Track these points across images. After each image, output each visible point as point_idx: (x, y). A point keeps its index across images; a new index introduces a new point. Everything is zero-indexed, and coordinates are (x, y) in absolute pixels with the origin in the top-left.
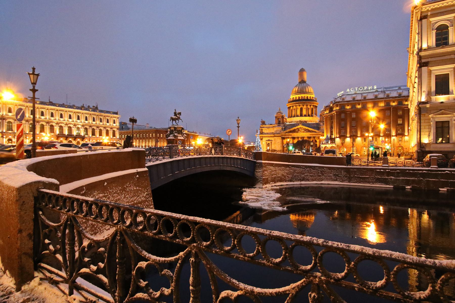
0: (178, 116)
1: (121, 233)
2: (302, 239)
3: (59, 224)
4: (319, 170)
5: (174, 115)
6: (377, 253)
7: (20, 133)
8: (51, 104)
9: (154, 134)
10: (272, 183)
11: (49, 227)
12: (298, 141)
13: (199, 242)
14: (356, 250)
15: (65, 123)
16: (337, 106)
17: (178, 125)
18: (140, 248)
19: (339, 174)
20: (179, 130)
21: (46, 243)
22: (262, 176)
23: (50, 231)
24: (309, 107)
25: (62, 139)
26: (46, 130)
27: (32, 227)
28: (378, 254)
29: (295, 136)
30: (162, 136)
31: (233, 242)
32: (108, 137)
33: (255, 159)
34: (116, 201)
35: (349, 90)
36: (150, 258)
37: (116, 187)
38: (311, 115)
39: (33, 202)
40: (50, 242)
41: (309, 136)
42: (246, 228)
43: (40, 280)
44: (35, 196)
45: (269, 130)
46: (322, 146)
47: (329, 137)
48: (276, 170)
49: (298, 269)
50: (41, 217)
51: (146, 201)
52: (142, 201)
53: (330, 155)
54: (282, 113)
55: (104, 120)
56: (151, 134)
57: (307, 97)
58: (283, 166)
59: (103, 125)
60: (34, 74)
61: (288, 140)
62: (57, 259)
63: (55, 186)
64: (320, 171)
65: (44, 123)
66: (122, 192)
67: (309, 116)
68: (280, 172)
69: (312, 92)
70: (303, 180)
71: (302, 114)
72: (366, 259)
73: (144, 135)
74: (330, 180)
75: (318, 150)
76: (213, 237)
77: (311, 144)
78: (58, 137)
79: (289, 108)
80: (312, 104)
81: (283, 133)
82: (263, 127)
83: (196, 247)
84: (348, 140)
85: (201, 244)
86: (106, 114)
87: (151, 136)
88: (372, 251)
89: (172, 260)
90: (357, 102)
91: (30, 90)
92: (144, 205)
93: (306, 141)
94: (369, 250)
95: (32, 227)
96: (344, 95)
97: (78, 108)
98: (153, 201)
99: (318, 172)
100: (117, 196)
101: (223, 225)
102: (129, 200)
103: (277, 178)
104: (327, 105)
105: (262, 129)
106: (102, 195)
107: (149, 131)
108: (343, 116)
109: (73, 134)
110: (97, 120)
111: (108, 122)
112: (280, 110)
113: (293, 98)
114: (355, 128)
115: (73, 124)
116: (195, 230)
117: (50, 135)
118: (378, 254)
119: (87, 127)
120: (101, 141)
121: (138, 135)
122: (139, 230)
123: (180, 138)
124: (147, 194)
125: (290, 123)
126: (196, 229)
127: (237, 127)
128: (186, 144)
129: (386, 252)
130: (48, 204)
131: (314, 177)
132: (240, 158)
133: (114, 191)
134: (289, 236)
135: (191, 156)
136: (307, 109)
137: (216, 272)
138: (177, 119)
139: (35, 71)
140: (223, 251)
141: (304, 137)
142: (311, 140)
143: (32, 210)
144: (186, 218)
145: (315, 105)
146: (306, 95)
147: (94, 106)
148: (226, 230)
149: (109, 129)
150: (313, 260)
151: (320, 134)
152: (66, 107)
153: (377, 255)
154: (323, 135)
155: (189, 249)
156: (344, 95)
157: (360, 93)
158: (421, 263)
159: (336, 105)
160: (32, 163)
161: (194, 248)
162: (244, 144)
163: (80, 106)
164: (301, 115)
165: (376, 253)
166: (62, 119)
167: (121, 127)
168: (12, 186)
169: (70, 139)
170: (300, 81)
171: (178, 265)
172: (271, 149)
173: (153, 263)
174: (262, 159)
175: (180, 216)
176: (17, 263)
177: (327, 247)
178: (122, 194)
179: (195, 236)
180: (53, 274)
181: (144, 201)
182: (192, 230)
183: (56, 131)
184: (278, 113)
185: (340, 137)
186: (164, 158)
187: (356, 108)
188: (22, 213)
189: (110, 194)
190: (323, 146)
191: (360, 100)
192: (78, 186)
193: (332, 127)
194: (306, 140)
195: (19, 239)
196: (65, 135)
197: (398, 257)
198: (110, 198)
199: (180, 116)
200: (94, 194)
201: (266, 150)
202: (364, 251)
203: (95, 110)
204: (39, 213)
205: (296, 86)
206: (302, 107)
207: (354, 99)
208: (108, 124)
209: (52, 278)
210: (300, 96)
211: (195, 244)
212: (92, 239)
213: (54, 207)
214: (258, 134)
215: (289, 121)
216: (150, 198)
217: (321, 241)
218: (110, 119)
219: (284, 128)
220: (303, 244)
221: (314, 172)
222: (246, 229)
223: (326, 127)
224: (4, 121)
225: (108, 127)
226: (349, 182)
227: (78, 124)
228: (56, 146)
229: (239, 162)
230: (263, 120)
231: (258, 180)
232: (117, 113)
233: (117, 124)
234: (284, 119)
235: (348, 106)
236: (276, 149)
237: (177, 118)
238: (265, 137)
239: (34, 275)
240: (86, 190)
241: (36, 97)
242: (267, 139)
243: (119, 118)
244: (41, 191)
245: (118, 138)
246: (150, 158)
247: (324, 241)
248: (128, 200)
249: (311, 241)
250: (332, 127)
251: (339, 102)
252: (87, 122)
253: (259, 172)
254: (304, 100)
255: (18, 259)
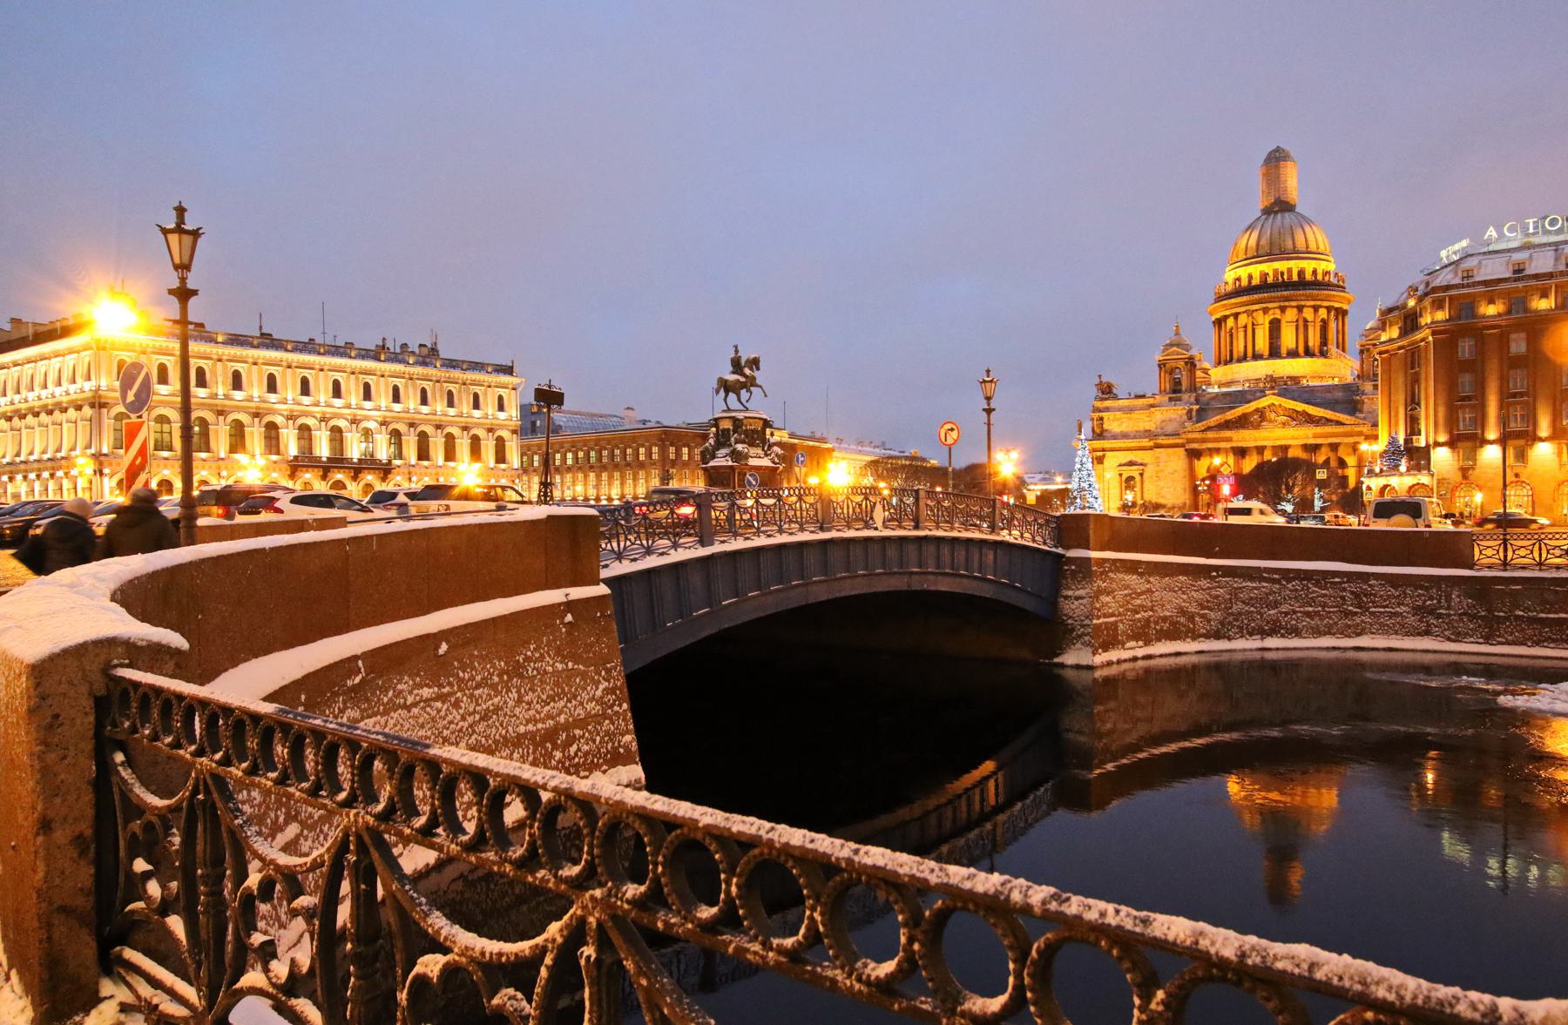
0: (747, 371)
1: (359, 837)
2: (967, 885)
3: (174, 800)
4: (1345, 590)
5: (731, 369)
6: (1254, 954)
7: (135, 458)
8: (268, 341)
9: (655, 449)
10: (1132, 644)
11: (145, 812)
12: (1260, 467)
13: (610, 884)
14: (1171, 938)
15: (318, 416)
16: (1438, 305)
17: (747, 409)
18: (423, 900)
19: (1441, 607)
20: (754, 431)
21: (136, 874)
22: (1090, 616)
23: (149, 827)
24: (1308, 314)
25: (308, 476)
26: (253, 445)
27: (89, 810)
28: (1258, 960)
29: (1244, 444)
30: (689, 454)
31: (723, 886)
32: (478, 466)
33: (1060, 542)
34: (486, 715)
35: (1494, 234)
36: (454, 942)
37: (483, 659)
38: (1317, 351)
39: (92, 718)
40: (150, 867)
41: (1312, 441)
42: (767, 833)
43: (121, 1011)
44: (98, 694)
45: (1129, 419)
46: (1367, 482)
47: (1402, 442)
48: (1149, 591)
49: (955, 1008)
50: (118, 772)
51: (605, 716)
52: (589, 715)
53: (1400, 523)
54: (1187, 348)
55: (460, 399)
56: (642, 450)
57: (1301, 273)
58: (1182, 574)
59: (429, 417)
60: (183, 230)
61: (1217, 460)
62: (169, 934)
63: (171, 658)
64: (1352, 593)
65: (244, 418)
66: (507, 682)
67: (1308, 353)
68: (1169, 598)
69: (1322, 248)
70: (1272, 632)
71: (1279, 347)
72: (1211, 979)
73: (617, 452)
74: (1396, 633)
75: (1352, 501)
76: (656, 864)
77: (1319, 477)
78: (295, 467)
79: (1219, 323)
80: (1326, 304)
81: (1194, 430)
82: (1107, 409)
83: (604, 904)
84: (1491, 454)
85: (618, 890)
86: (471, 376)
87: (642, 458)
88: (1237, 944)
89: (523, 951)
90: (1533, 283)
91: (171, 292)
92: (598, 734)
93: (1296, 464)
94: (1226, 939)
95: (90, 812)
96: (1472, 255)
97: (365, 354)
98: (634, 717)
99: (1343, 598)
100: (489, 695)
101: (690, 818)
102: (536, 711)
103: (1156, 623)
104: (1390, 303)
105: (1101, 419)
106: (431, 690)
107: (634, 439)
108: (1466, 348)
109: (349, 456)
110: (438, 398)
111: (476, 406)
112: (1177, 334)
113: (1239, 279)
114: (1527, 403)
115: (349, 417)
116: (597, 833)
117: (267, 459)
118: (1258, 960)
119: (402, 428)
120: (453, 481)
121: (593, 454)
122: (417, 830)
123: (759, 460)
124: (607, 691)
125: (1225, 390)
126: (600, 831)
127: (984, 410)
128: (785, 485)
129: (1296, 953)
130: (139, 725)
131: (1321, 620)
132: (996, 543)
133: (478, 678)
134: (922, 872)
135: (784, 535)
136: (1301, 323)
137: (670, 1006)
138: (744, 386)
139: (186, 222)
140: (693, 923)
141: (1285, 448)
142: (1321, 459)
143: (89, 746)
144: (564, 786)
145: (1337, 305)
146: (1295, 265)
147: (425, 346)
148: (699, 836)
149: (481, 433)
150: (1010, 974)
151: (1360, 434)
152: (322, 351)
153: (1255, 965)
154: (1376, 438)
155: (579, 912)
156: (1472, 255)
157: (1550, 244)
158: (1433, 1010)
159: (1433, 302)
160: (150, 569)
161: (594, 908)
162: (1021, 483)
163: (373, 348)
164: (1274, 353)
165: (1250, 957)
166: (306, 400)
167: (529, 425)
168: (16, 655)
169: (339, 476)
170: (1266, 203)
171: (544, 972)
172: (1140, 502)
173: (464, 960)
174: (1087, 541)
175: (547, 778)
176: (37, 944)
177: (1060, 918)
178: (509, 690)
179: (597, 861)
180: (159, 991)
181: (596, 715)
182: (588, 835)
183: (286, 447)
184: (1171, 345)
185: (1452, 444)
186: (675, 546)
187: (1526, 310)
188: (52, 757)
189: (460, 689)
190: (1375, 483)
191: (1550, 275)
192: (337, 659)
193: (1413, 401)
194: (1296, 461)
195: (42, 853)
196: (318, 459)
197: (1341, 978)
198: (462, 705)
199: (756, 374)
200: (399, 687)
201: (1118, 504)
202: (1204, 944)
203: (428, 360)
204: (113, 759)
205: (1249, 227)
206: (1279, 317)
207: (1519, 270)
208: (477, 413)
209: (157, 1006)
210: (1269, 268)
211: (598, 893)
212: (272, 862)
213: (155, 737)
214: (1083, 437)
215: (1219, 378)
216: (620, 705)
217: (1039, 894)
218: (485, 394)
219: (1198, 411)
220: (971, 906)
221: (1325, 595)
222: (770, 835)
223: (1386, 400)
224: (105, 411)
225: (478, 425)
226: (1488, 639)
227: (367, 418)
228: (277, 505)
229: (991, 557)
230: (1104, 380)
231: (1073, 630)
232: (512, 367)
233: (512, 413)
234: (1199, 374)
235: (1491, 301)
236: (1162, 501)
237: (742, 379)
238: (1112, 450)
239: (97, 991)
240: (367, 675)
241: (191, 318)
242: (1127, 457)
243: (520, 389)
244: (118, 674)
245: (516, 467)
246: (619, 545)
247: (1053, 896)
248: (532, 712)
249: (1001, 893)
250: (1413, 401)
251: (1448, 288)
252: (397, 407)
253: (1077, 598)
254: (1275, 286)
255: (41, 928)
